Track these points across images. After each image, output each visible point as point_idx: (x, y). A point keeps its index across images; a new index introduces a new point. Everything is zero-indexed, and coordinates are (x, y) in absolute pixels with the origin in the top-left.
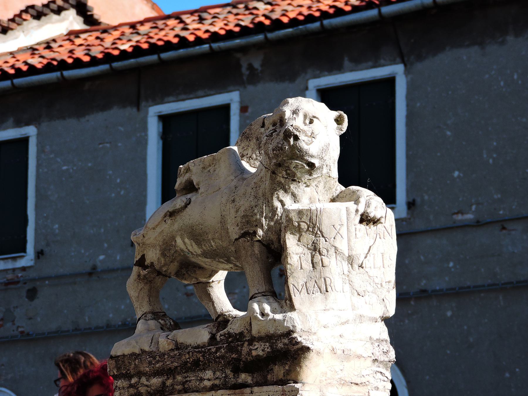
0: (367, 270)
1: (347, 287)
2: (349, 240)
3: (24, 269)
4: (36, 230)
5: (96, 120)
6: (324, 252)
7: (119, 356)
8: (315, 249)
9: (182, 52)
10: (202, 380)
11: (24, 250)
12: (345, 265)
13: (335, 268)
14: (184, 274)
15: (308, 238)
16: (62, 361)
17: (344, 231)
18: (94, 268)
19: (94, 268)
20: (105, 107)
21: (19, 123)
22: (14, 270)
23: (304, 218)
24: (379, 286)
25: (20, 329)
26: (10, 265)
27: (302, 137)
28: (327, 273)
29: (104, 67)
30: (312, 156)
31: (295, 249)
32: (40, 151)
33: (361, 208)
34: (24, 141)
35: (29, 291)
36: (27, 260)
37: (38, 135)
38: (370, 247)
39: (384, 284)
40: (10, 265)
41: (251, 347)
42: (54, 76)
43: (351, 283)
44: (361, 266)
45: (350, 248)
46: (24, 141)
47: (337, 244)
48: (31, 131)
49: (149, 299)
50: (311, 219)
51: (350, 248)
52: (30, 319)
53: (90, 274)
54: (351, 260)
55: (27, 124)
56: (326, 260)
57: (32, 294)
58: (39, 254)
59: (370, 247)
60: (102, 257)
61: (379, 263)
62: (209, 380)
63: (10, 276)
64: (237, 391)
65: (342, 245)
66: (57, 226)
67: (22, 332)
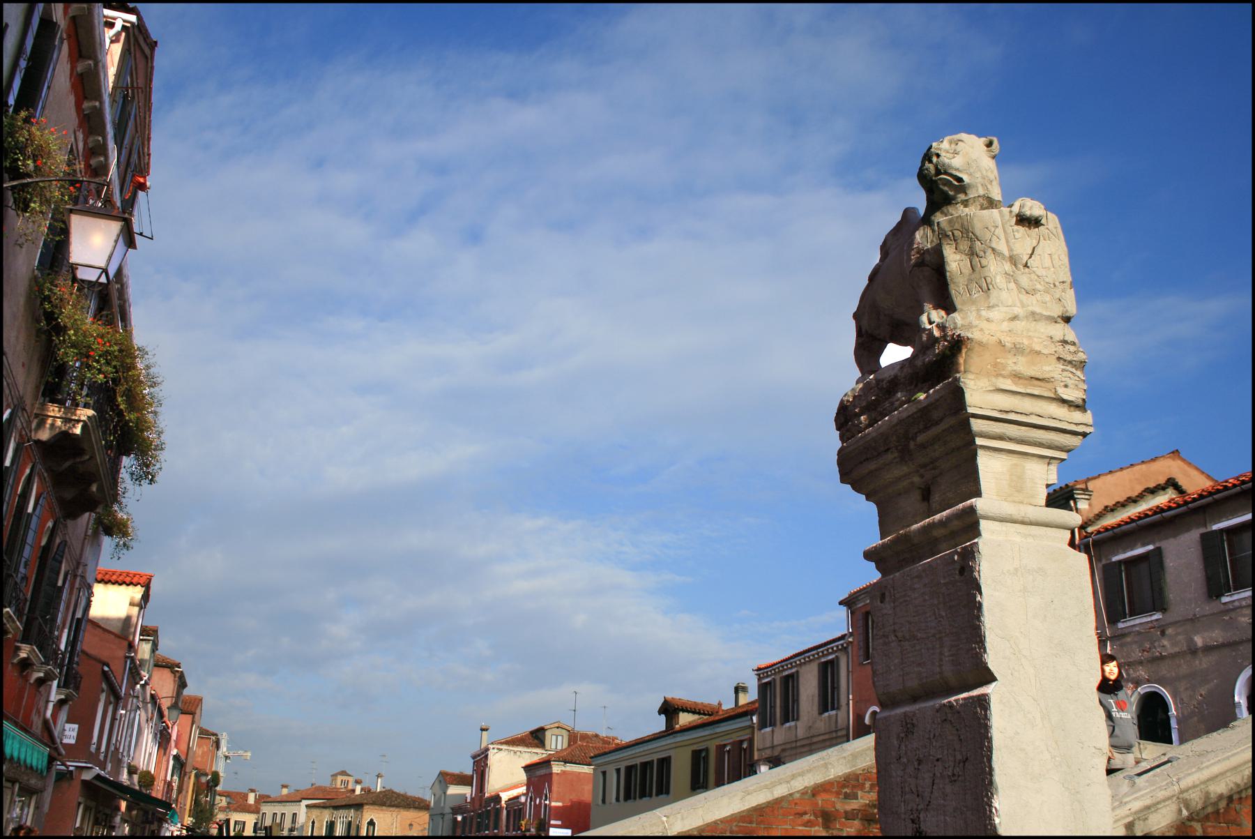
1: (1012, 285)
2: (1007, 242)
6: (981, 254)
8: (972, 253)
9: (1226, 493)
12: (1008, 267)
13: (995, 268)
15: (964, 245)
16: (1113, 620)
17: (999, 232)
23: (957, 226)
27: (943, 154)
28: (985, 272)
29: (1184, 508)
30: (957, 169)
31: (954, 261)
33: (1016, 209)
40: (1149, 619)
43: (1016, 282)
44: (1026, 266)
45: (1010, 250)
47: (994, 245)
50: (962, 225)
51: (1010, 250)
54: (1013, 260)
56: (984, 262)
61: (1047, 263)
65: (1002, 247)
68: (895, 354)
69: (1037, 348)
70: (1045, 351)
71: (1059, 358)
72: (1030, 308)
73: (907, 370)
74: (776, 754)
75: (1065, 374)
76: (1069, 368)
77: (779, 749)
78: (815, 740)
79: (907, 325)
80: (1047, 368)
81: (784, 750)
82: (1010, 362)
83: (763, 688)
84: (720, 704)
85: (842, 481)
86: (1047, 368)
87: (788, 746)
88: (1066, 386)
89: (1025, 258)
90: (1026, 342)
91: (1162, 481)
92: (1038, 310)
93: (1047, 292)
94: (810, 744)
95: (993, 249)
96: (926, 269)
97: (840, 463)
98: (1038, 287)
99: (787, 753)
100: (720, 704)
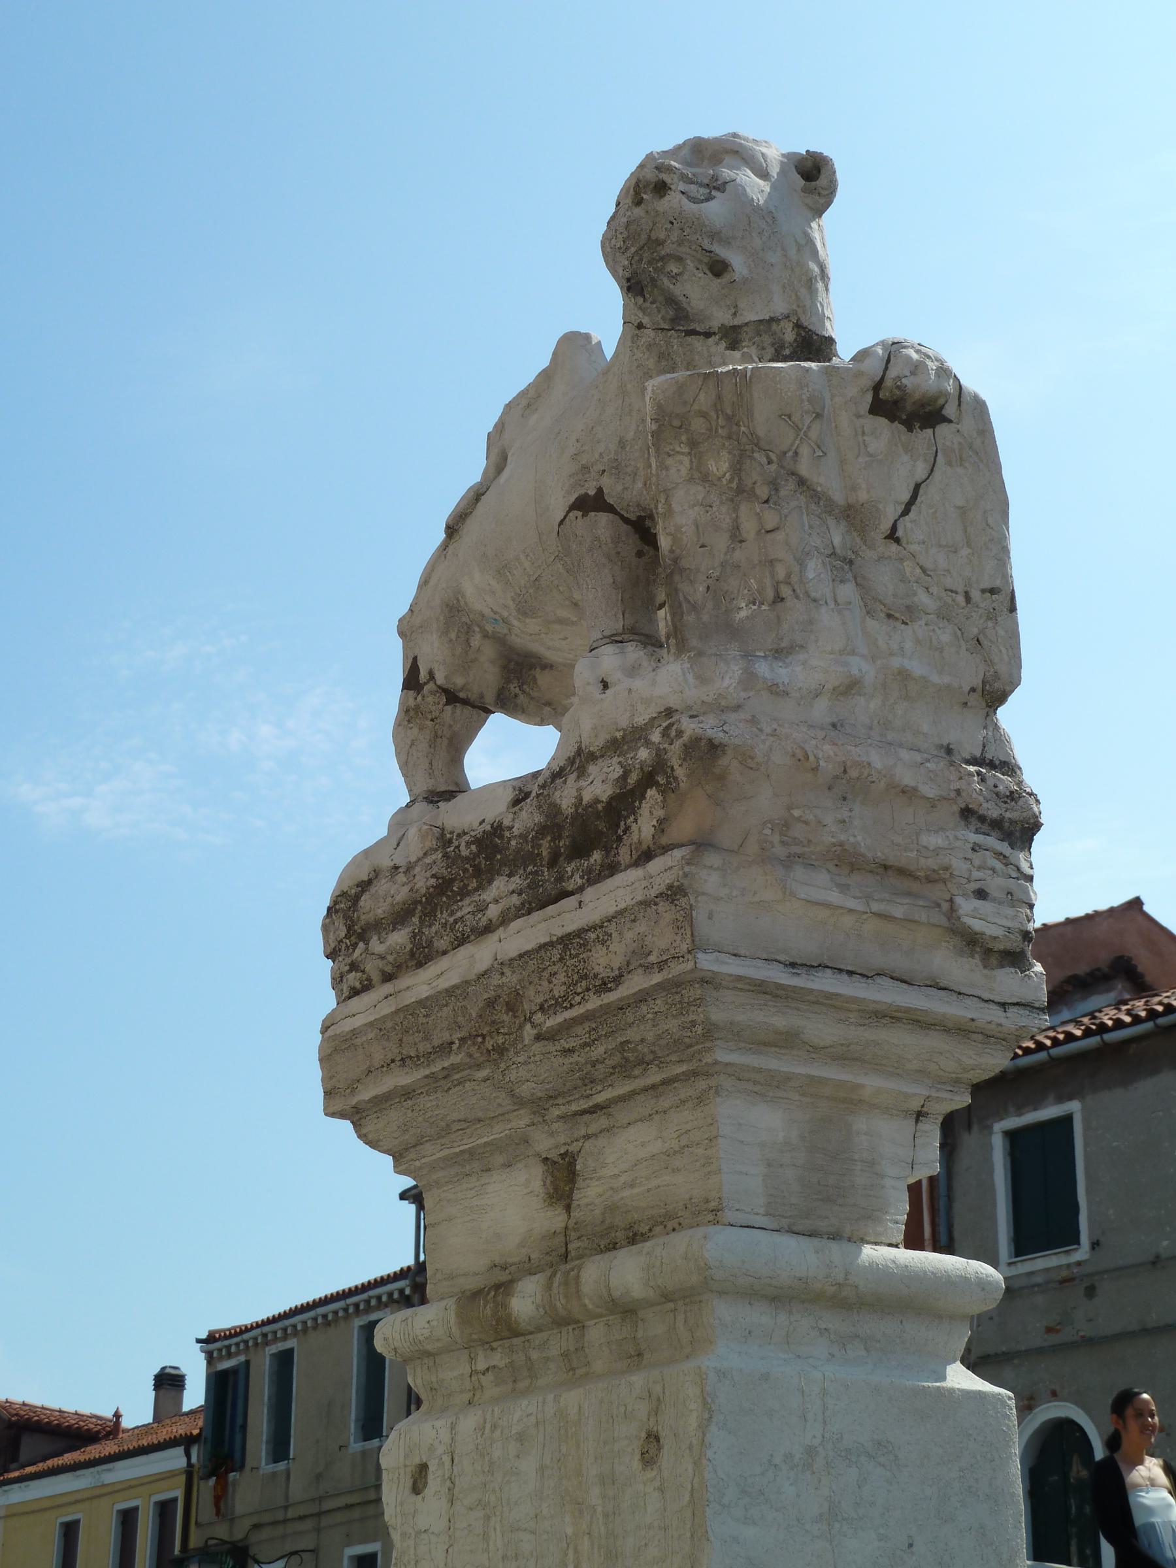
0: (914, 548)
3: (1079, 1264)
4: (1089, 1219)
5: (1146, 1088)
7: (485, 974)
10: (482, 908)
11: (1077, 1241)
14: (516, 696)
18: (1158, 1257)
19: (1158, 1257)
20: (1155, 1071)
21: (1060, 1099)
22: (1068, 1266)
24: (961, 599)
25: (1081, 1334)
26: (1063, 1260)
29: (1150, 1025)
30: (715, 235)
32: (1087, 1128)
34: (1068, 1120)
35: (1086, 1288)
36: (1082, 1253)
37: (1083, 1109)
38: (917, 487)
39: (975, 595)
40: (1063, 1260)
41: (582, 783)
42: (1094, 1041)
43: (861, 583)
46: (1068, 1120)
48: (1074, 1106)
49: (431, 764)
52: (1091, 1320)
53: (1154, 1263)
55: (1070, 1099)
57: (1091, 1292)
58: (1095, 1245)
59: (917, 487)
60: (1165, 1243)
62: (496, 901)
63: (1065, 1273)
64: (551, 909)
66: (1111, 1211)
67: (1082, 1337)
68: (506, 752)
69: (907, 778)
70: (929, 791)
71: (967, 813)
72: (896, 662)
73: (528, 818)
74: (238, 1535)
75: (977, 859)
76: (992, 841)
77: (247, 1524)
78: (328, 1505)
79: (547, 666)
80: (934, 841)
81: (256, 1527)
82: (829, 819)
83: (222, 1385)
84: (117, 1415)
85: (330, 1113)
86: (934, 841)
87: (266, 1518)
88: (981, 894)
89: (891, 513)
90: (877, 760)
91: (1103, 958)
92: (917, 668)
93: (944, 615)
94: (319, 1514)
95: (802, 482)
96: (603, 518)
97: (327, 1059)
98: (923, 598)
99: (266, 1533)
100: (117, 1415)
